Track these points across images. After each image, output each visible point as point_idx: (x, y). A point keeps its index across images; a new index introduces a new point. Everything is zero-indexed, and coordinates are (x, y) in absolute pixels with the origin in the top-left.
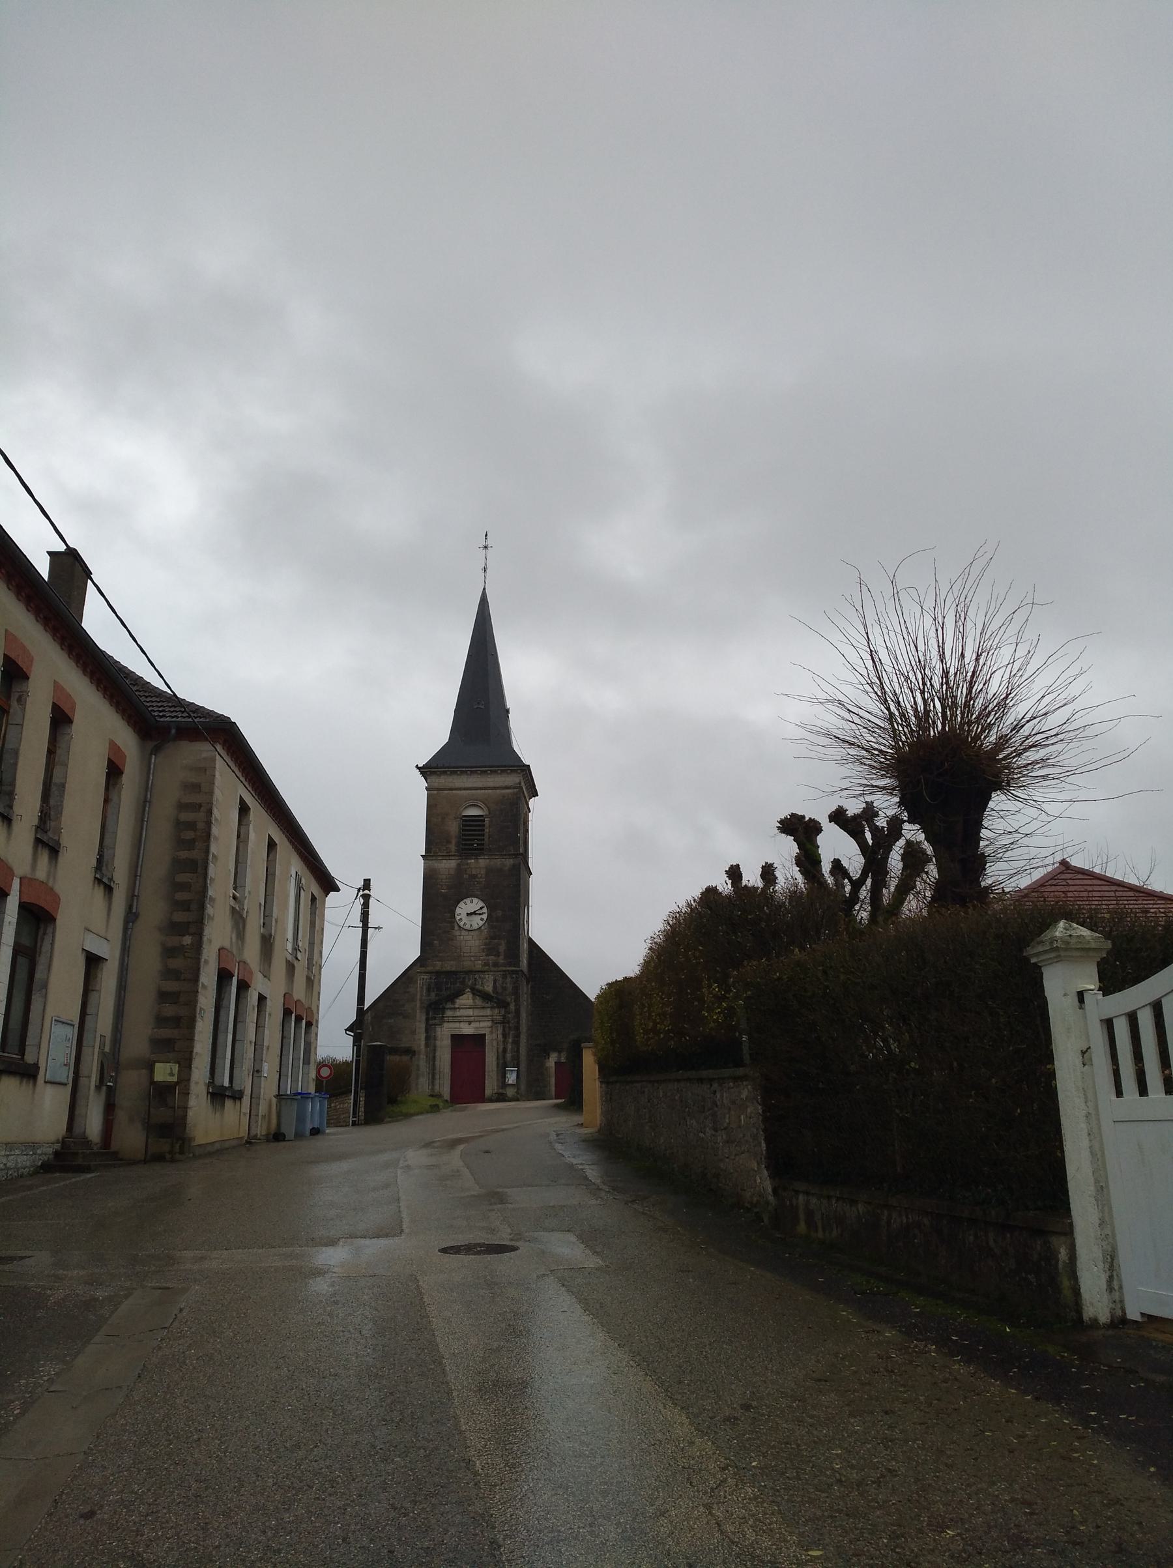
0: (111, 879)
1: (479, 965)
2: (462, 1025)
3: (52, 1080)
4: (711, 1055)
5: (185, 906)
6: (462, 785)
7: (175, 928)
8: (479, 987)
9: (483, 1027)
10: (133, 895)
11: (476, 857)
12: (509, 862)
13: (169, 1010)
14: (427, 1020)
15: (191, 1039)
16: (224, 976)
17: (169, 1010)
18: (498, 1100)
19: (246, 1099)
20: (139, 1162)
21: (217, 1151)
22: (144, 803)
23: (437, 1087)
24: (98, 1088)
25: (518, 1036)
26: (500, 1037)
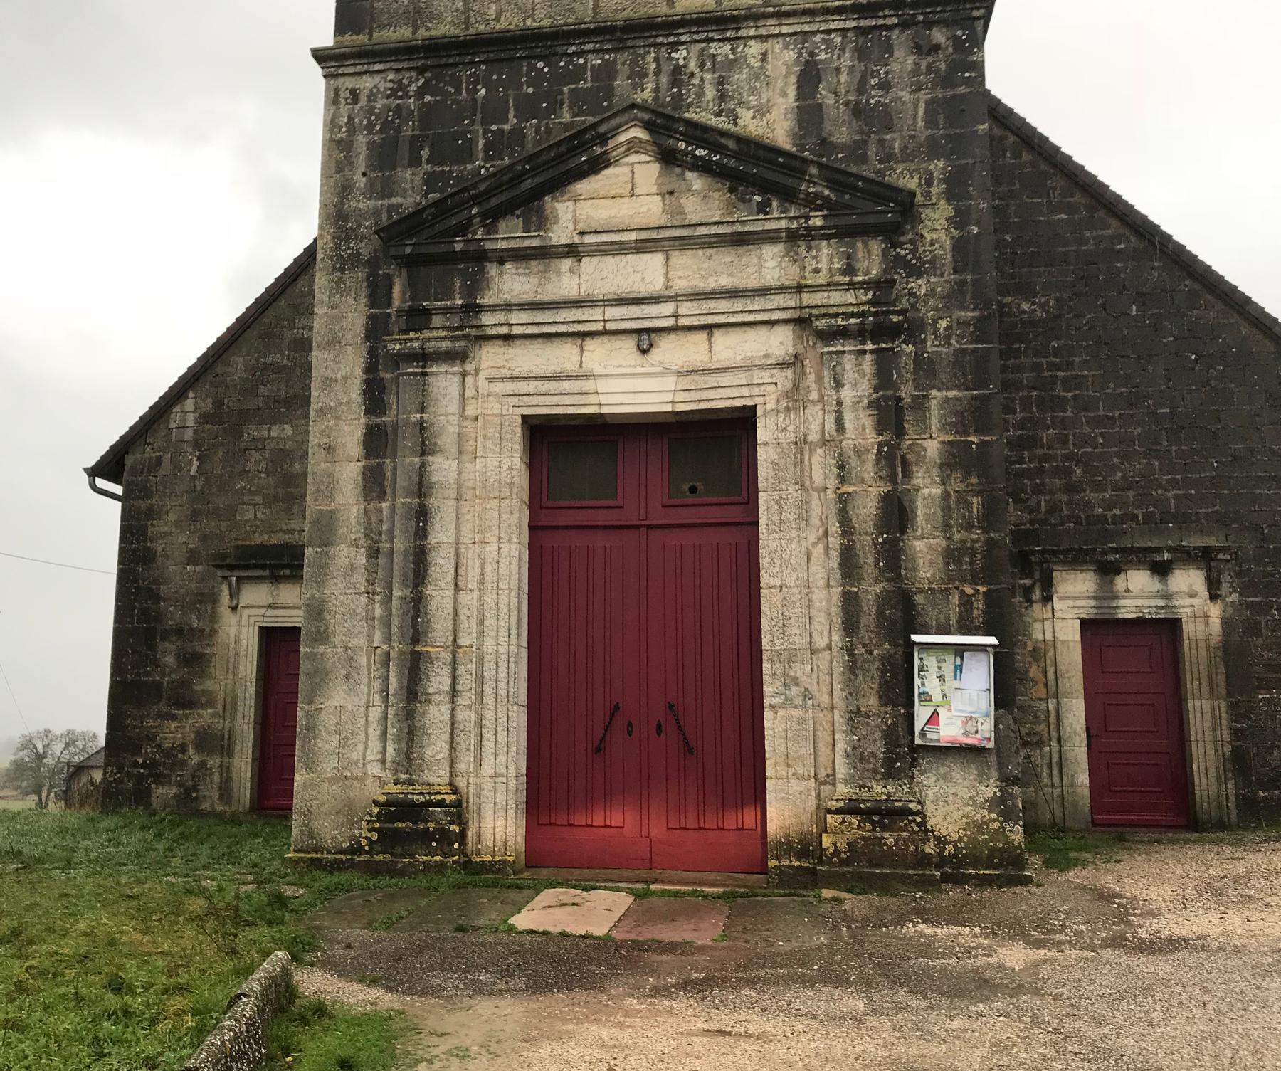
2: (598, 355)
9: (736, 364)
14: (376, 330)
23: (436, 748)
26: (861, 429)
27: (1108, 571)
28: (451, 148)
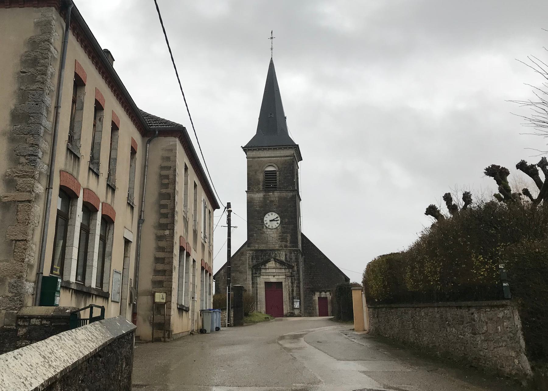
0: (133, 203)
1: (277, 247)
3: (114, 300)
4: (487, 294)
5: (165, 216)
6: (262, 156)
7: (161, 226)
8: (278, 258)
10: (142, 211)
11: (273, 191)
12: (290, 194)
13: (160, 267)
14: (252, 274)
15: (170, 281)
16: (182, 249)
17: (160, 267)
18: (290, 316)
19: (190, 312)
20: (150, 342)
21: (181, 338)
22: (145, 167)
24: (129, 304)
25: (299, 283)
26: (290, 284)
27: (321, 292)
28: (258, 259)
